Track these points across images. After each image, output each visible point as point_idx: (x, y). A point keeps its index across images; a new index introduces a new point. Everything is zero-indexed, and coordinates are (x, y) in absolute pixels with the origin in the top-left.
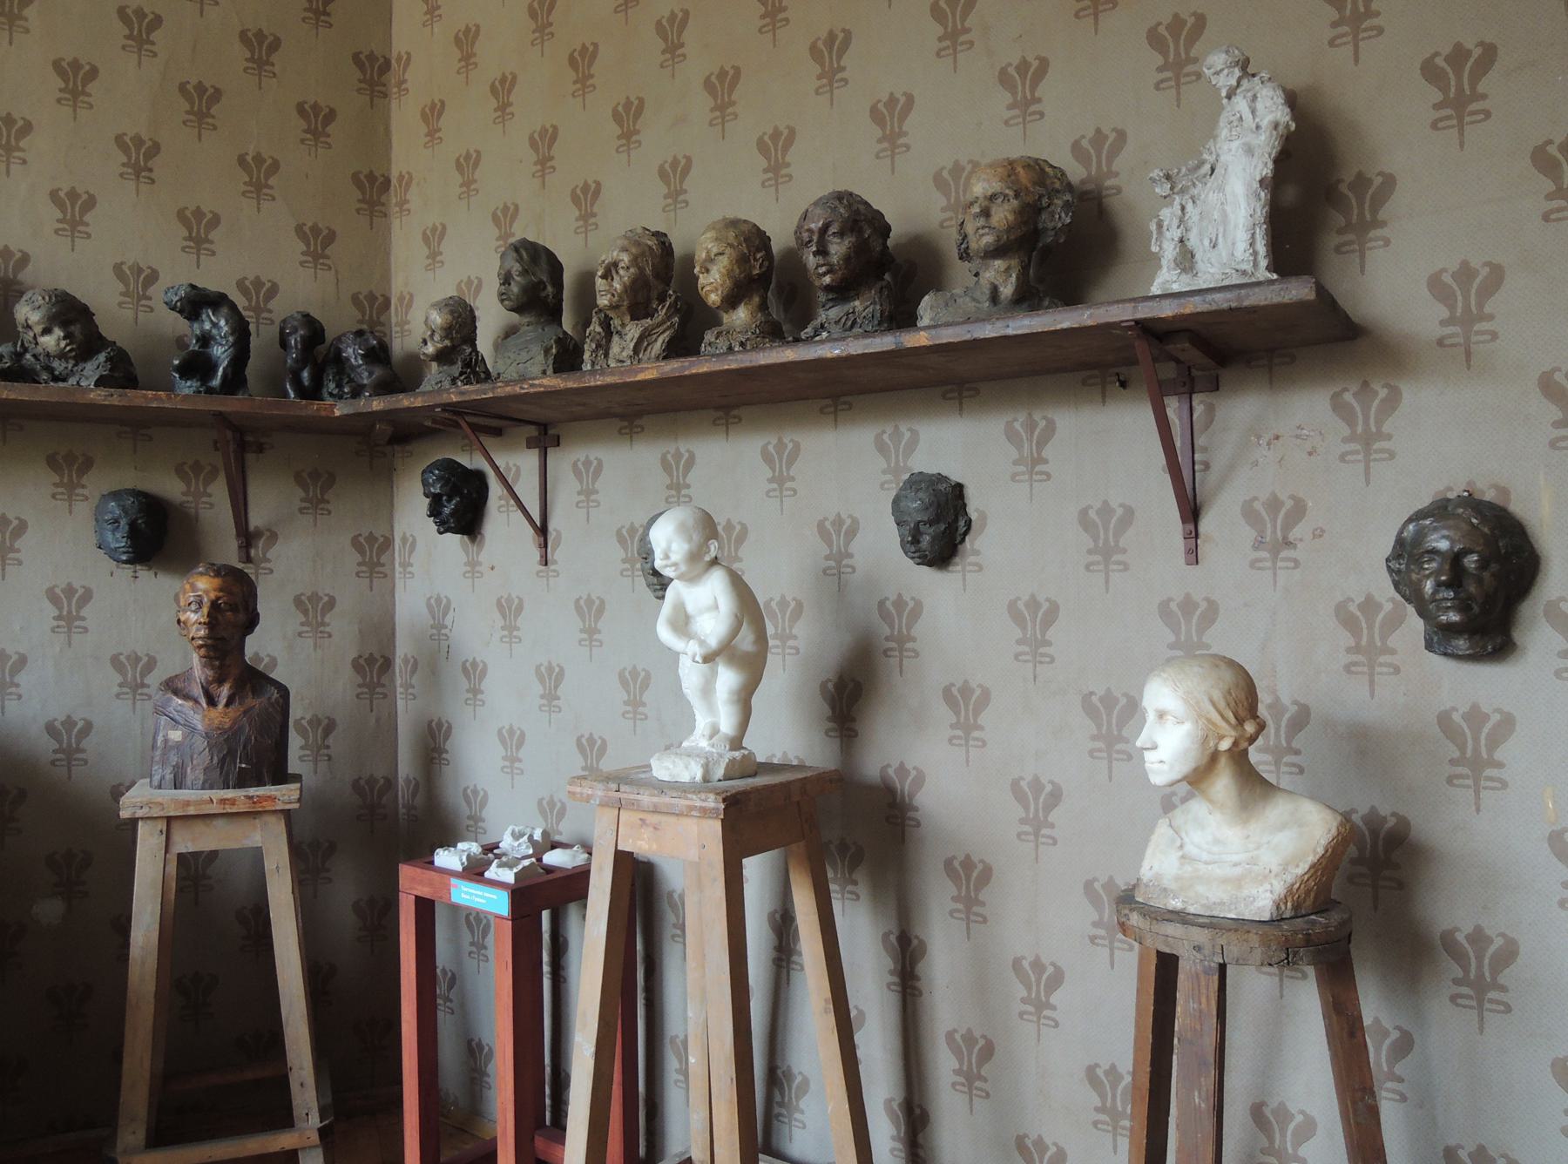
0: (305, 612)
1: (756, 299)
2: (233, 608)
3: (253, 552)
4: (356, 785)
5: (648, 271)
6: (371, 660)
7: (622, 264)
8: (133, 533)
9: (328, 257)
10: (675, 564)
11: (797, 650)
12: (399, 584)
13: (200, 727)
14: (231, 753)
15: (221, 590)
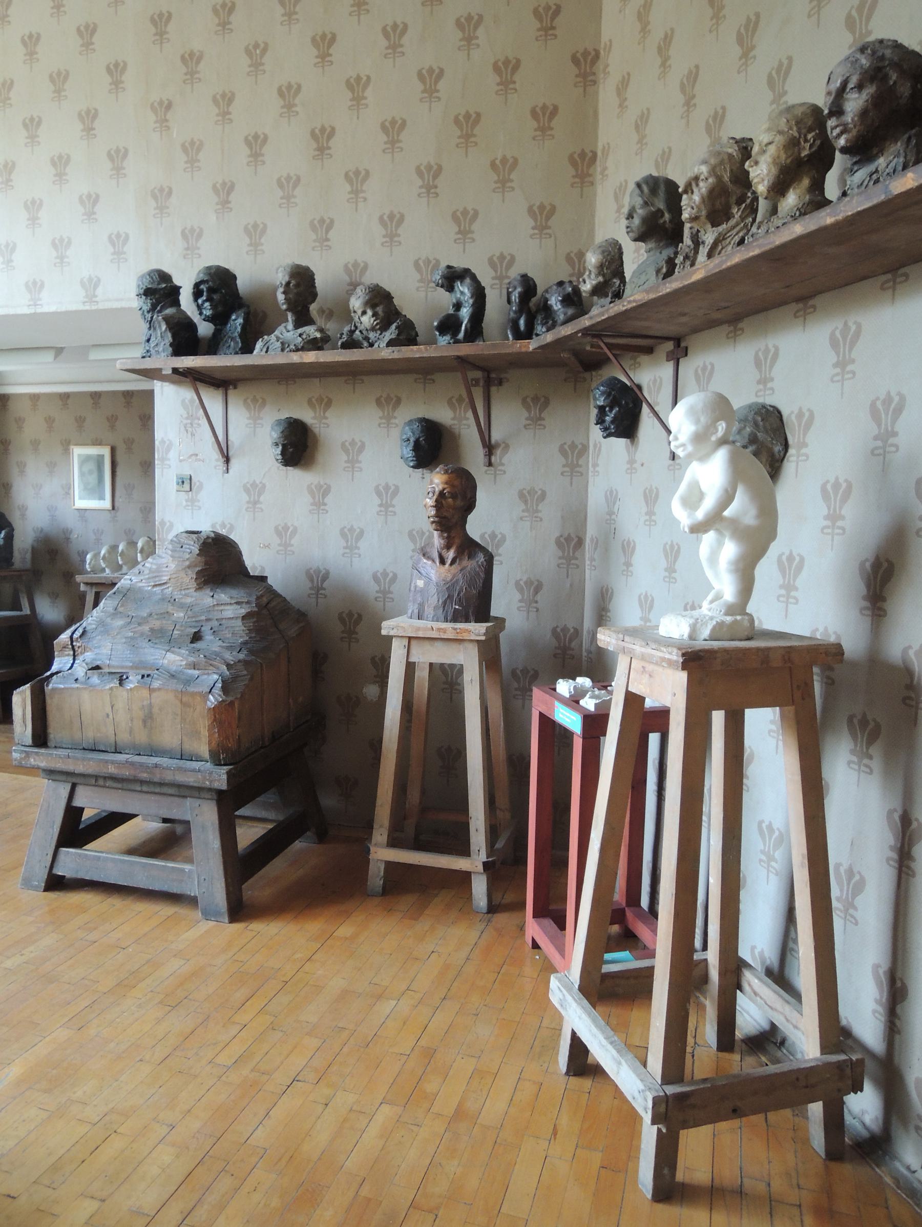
0: (526, 502)
1: (806, 182)
2: (454, 496)
3: (493, 459)
4: (554, 631)
5: (726, 178)
6: (568, 539)
7: (702, 177)
8: (417, 447)
9: (549, 228)
10: (683, 445)
11: (843, 529)
12: (591, 480)
13: (434, 579)
14: (450, 597)
15: (446, 483)
